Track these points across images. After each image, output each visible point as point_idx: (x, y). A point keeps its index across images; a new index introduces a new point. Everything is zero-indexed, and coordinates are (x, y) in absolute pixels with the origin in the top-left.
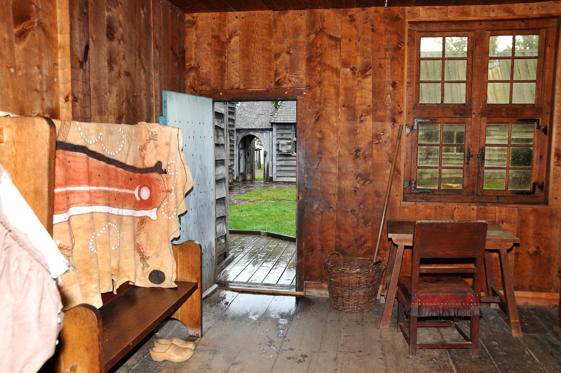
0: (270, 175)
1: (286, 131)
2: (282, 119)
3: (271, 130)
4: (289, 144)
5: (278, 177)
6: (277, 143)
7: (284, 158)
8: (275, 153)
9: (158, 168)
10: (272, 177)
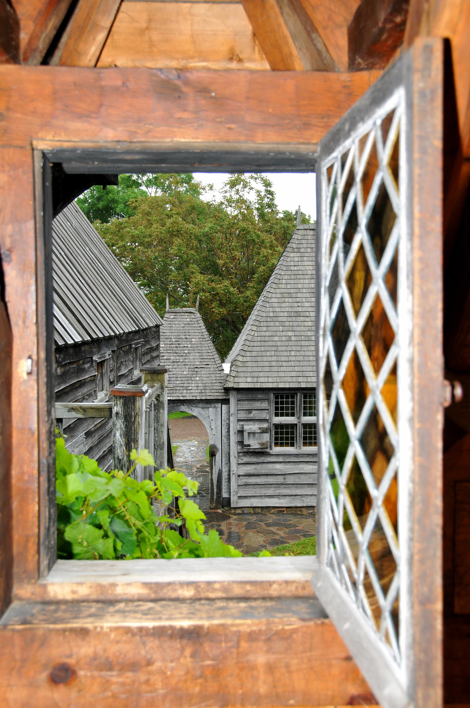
0: (225, 495)
1: (258, 405)
2: (249, 380)
3: (226, 401)
4: (264, 431)
5: (240, 497)
6: (239, 428)
7: (254, 459)
8: (234, 449)
10: (229, 500)
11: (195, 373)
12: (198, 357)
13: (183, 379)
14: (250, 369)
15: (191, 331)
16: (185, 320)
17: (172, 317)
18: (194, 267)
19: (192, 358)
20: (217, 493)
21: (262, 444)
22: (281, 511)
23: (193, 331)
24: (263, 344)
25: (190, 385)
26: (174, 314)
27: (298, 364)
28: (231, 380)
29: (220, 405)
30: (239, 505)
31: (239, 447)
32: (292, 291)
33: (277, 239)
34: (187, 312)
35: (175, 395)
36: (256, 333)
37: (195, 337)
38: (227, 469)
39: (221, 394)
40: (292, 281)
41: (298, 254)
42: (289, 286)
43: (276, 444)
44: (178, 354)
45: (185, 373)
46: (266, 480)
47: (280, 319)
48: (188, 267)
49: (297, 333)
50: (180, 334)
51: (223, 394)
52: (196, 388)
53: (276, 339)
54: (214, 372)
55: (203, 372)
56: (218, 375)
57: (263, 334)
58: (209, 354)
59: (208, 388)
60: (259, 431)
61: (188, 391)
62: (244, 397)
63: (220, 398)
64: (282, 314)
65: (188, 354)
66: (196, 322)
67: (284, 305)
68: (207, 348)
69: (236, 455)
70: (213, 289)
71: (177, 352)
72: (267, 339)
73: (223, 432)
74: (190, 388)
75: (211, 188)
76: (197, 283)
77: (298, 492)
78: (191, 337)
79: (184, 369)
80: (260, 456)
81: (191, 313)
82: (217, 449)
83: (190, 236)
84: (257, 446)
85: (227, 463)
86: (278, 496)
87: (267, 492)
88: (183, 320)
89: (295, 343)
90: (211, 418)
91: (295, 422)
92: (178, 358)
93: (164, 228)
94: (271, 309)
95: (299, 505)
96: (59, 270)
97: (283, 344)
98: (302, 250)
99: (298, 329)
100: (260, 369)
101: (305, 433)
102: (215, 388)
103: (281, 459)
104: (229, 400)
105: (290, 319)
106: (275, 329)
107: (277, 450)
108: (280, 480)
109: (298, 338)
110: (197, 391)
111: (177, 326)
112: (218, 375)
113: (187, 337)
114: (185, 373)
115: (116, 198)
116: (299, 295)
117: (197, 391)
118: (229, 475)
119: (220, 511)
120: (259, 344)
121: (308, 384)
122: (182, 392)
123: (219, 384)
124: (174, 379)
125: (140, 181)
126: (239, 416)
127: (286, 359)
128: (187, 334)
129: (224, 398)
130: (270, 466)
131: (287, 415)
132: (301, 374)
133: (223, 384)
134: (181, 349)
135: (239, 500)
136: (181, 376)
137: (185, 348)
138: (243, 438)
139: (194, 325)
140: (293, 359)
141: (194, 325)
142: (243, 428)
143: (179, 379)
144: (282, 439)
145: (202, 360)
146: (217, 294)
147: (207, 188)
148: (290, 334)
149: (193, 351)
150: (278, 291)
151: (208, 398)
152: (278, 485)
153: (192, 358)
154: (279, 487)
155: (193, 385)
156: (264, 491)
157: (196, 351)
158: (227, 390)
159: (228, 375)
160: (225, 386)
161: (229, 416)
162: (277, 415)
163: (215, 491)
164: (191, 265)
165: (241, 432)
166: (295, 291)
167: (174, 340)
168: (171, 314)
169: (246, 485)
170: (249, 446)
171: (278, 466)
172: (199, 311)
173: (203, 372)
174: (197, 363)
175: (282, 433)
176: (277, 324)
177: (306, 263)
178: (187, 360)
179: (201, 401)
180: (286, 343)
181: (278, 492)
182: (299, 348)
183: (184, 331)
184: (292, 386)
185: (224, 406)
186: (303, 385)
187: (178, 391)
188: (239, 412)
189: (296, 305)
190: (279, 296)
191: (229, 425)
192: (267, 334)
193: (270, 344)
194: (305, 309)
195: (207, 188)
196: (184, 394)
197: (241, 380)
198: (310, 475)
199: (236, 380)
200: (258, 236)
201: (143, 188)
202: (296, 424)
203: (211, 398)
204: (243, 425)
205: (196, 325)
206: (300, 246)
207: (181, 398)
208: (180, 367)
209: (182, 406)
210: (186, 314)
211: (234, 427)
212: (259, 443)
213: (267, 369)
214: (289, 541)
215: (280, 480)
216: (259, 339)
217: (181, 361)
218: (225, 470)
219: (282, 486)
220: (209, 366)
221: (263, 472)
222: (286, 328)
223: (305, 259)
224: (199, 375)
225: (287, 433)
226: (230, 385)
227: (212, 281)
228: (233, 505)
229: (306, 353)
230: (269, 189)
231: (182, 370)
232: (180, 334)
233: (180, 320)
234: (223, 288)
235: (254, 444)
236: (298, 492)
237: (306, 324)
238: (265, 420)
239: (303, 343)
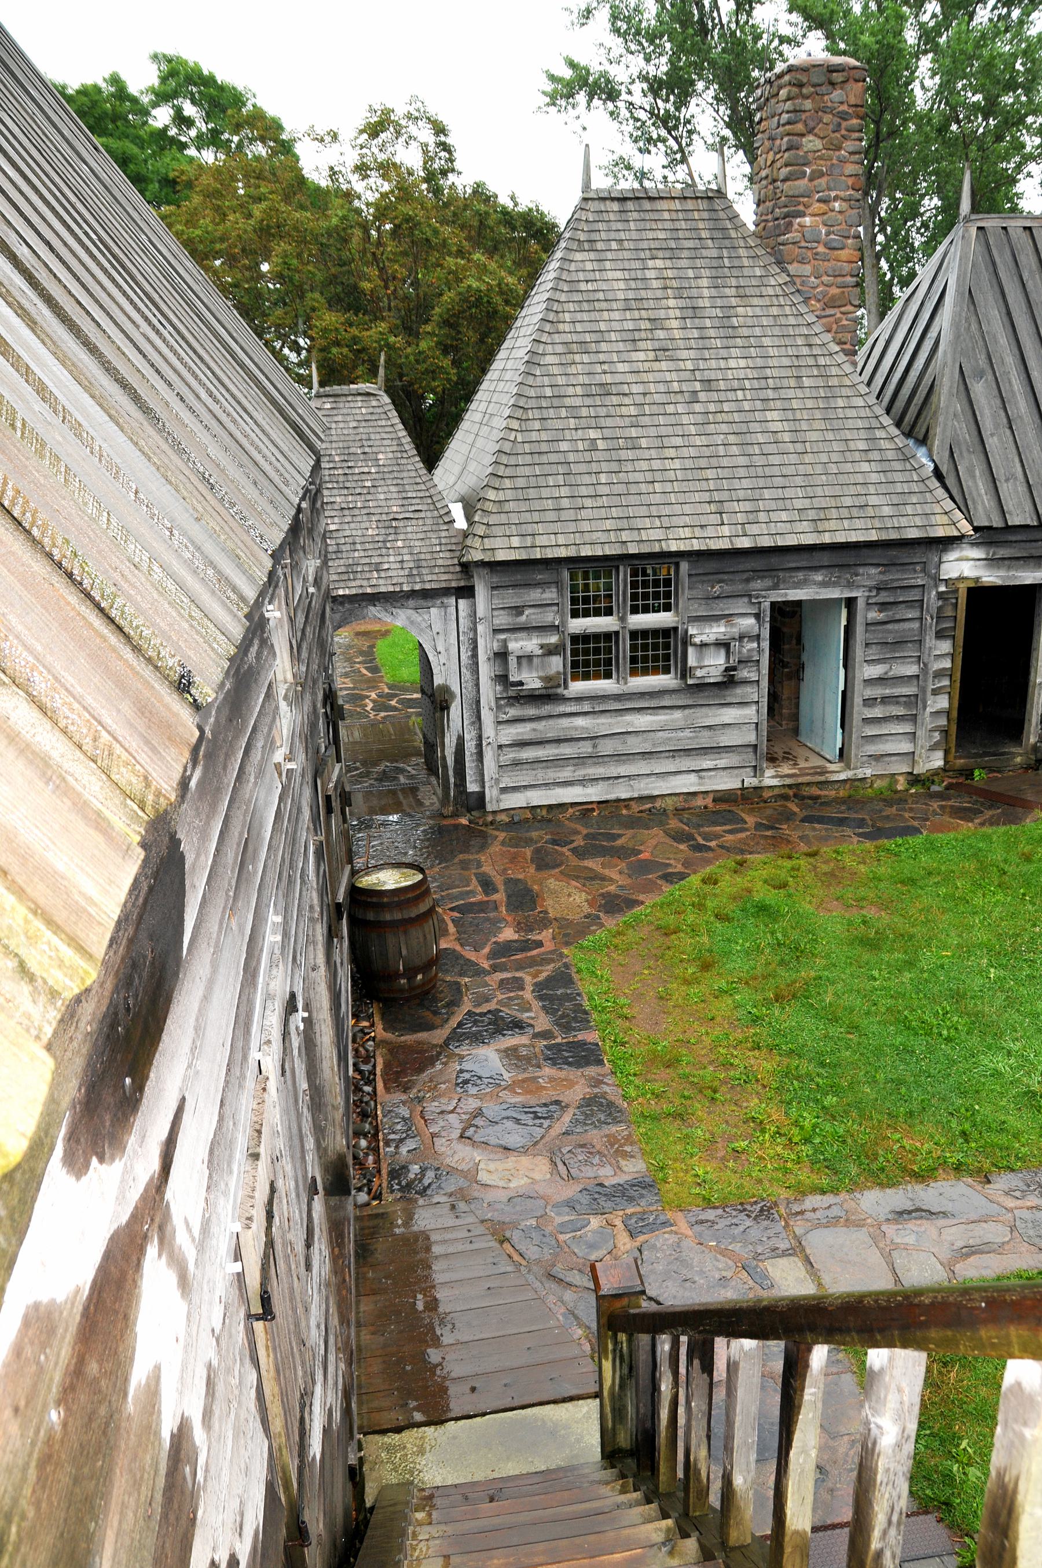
0: (472, 787)
1: (535, 595)
2: (516, 542)
3: (467, 592)
4: (550, 651)
5: (504, 790)
6: (496, 646)
7: (531, 711)
8: (488, 691)
9: (331, 168)
10: (481, 796)
11: (392, 531)
12: (395, 495)
13: (367, 546)
14: (514, 518)
15: (373, 437)
16: (358, 411)
17: (328, 406)
18: (315, 298)
19: (382, 497)
20: (455, 785)
21: (546, 679)
22: (588, 810)
23: (378, 437)
24: (536, 459)
25: (386, 559)
26: (331, 399)
27: (616, 501)
28: (477, 545)
29: (453, 600)
30: (503, 806)
31: (498, 688)
32: (588, 338)
33: (469, 238)
34: (360, 394)
35: (353, 584)
36: (519, 435)
37: (383, 449)
38: (474, 733)
39: (454, 577)
40: (585, 316)
41: (592, 255)
42: (579, 327)
43: (575, 678)
44: (351, 491)
45: (370, 532)
46: (556, 751)
47: (568, 402)
48: (302, 297)
49: (607, 433)
50: (351, 444)
51: (459, 576)
52: (398, 566)
53: (564, 446)
54: (434, 528)
55: (409, 529)
56: (443, 534)
57: (534, 436)
58: (419, 487)
59: (424, 564)
60: (540, 652)
61: (383, 574)
62: (506, 579)
63: (454, 584)
64: (570, 391)
65: (372, 490)
66: (384, 416)
67: (573, 370)
68: (413, 474)
69: (493, 704)
70: (355, 340)
71: (348, 485)
72: (544, 447)
73: (463, 657)
74: (386, 566)
75: (335, 137)
76: (325, 330)
77: (623, 770)
78: (374, 449)
79: (367, 525)
80: (544, 703)
81: (368, 394)
82: (452, 695)
83: (302, 237)
84: (537, 684)
85: (473, 723)
86: (582, 782)
87: (560, 775)
88: (354, 411)
89: (606, 455)
90: (435, 629)
91: (616, 628)
92: (350, 498)
93: (252, 222)
94: (546, 381)
95: (624, 796)
96: (98, 288)
97: (580, 457)
98: (600, 246)
99: (609, 422)
100: (536, 517)
101: (634, 648)
102: (440, 562)
103: (586, 707)
104: (473, 587)
105: (588, 401)
106: (559, 424)
107: (578, 687)
108: (586, 748)
109: (611, 444)
110: (402, 573)
111: (341, 425)
112: (443, 534)
113: (367, 450)
114: (370, 532)
115: (144, 171)
116: (604, 347)
117: (402, 573)
118: (479, 746)
119: (464, 821)
120: (528, 459)
121: (641, 545)
122: (368, 575)
123: (448, 555)
124: (348, 547)
125: (183, 139)
126: (496, 621)
127: (590, 491)
128: (365, 443)
129: (462, 584)
130: (565, 722)
131: (597, 613)
132: (624, 524)
133: (458, 554)
134: (356, 478)
135: (503, 796)
136: (363, 540)
137: (364, 477)
138: (507, 669)
139: (380, 423)
140: (605, 490)
141: (380, 423)
142: (506, 647)
143: (358, 547)
144: (586, 664)
145: (405, 502)
146: (363, 350)
147: (328, 139)
148: (593, 434)
149: (382, 482)
150: (557, 338)
151: (428, 586)
152: (580, 760)
153: (382, 497)
154: (584, 764)
155: (392, 559)
156: (552, 775)
157: (389, 482)
158: (466, 568)
159: (465, 535)
160: (465, 559)
161: (475, 624)
162: (575, 614)
163: (452, 780)
164: (309, 295)
165: (502, 656)
166: (594, 337)
167: (337, 459)
168: (324, 399)
169: (516, 764)
170: (521, 683)
171: (580, 722)
172: (386, 391)
173: (409, 529)
174: (395, 509)
175: (586, 652)
176: (563, 413)
177: (610, 275)
178: (371, 504)
179: (413, 594)
180: (587, 456)
181: (581, 773)
182: (614, 466)
183: (358, 438)
184: (608, 551)
185: (462, 603)
186: (633, 549)
187: (359, 576)
188: (495, 613)
189: (598, 368)
190: (560, 349)
191: (475, 642)
192: (544, 436)
193: (553, 458)
194: (618, 378)
195: (328, 139)
196: (374, 582)
197: (497, 543)
198: (645, 735)
199: (488, 543)
200: (436, 232)
201: (192, 152)
202: (617, 633)
203: (434, 586)
204: (505, 641)
205: (383, 423)
206: (595, 236)
207: (369, 590)
208: (359, 519)
209: (372, 608)
210: (359, 398)
211: (486, 646)
212: (540, 678)
213: (552, 516)
214: (641, 897)
215: (586, 748)
216: (527, 448)
217: (359, 505)
218: (469, 737)
219: (590, 761)
220: (422, 515)
221: (550, 735)
222: (583, 423)
223: (608, 265)
224: (402, 537)
225: (597, 651)
226: (477, 556)
227: (351, 325)
228: (489, 808)
229: (632, 477)
230: (443, 138)
231: (363, 525)
232: (351, 444)
233: (345, 411)
234: (376, 337)
235: (532, 681)
236: (623, 770)
237: (624, 410)
238: (553, 628)
239: (624, 454)
